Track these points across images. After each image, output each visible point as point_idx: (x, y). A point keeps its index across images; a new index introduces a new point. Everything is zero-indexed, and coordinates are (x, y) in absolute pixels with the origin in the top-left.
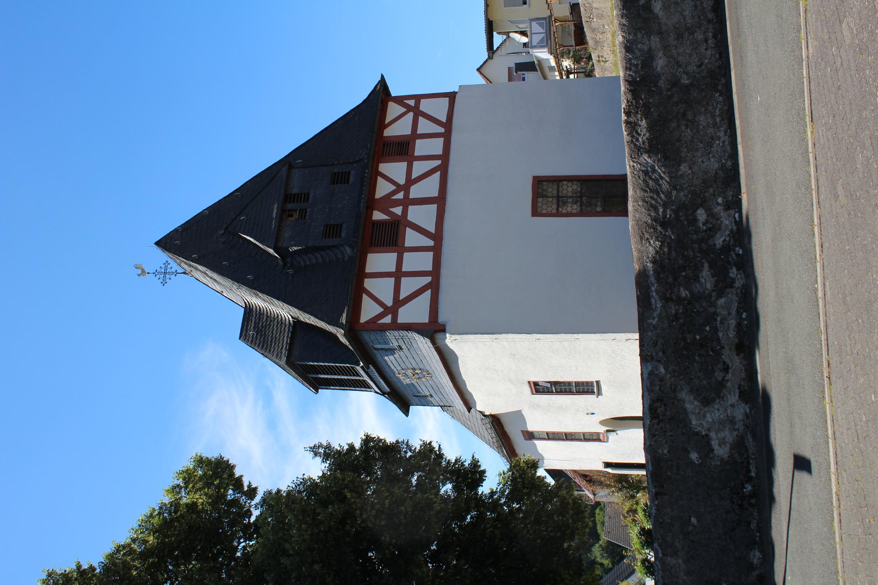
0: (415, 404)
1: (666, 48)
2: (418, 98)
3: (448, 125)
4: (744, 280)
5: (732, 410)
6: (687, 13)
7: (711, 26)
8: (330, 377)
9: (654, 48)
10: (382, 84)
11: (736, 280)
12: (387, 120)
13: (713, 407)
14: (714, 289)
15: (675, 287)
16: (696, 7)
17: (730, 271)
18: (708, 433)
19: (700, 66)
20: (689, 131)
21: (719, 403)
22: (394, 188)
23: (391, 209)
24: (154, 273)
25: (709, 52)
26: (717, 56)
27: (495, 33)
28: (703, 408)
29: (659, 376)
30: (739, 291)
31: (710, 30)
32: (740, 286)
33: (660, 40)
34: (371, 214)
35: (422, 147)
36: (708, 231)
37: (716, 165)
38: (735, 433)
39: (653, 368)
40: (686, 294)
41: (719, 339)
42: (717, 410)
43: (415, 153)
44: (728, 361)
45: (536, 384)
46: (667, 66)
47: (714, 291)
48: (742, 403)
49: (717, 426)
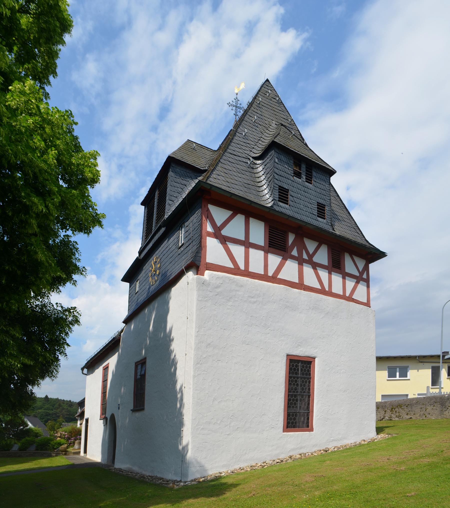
0: (129, 308)
8: (154, 221)
23: (295, 248)
24: (237, 98)
34: (293, 232)
35: (337, 279)
43: (333, 273)
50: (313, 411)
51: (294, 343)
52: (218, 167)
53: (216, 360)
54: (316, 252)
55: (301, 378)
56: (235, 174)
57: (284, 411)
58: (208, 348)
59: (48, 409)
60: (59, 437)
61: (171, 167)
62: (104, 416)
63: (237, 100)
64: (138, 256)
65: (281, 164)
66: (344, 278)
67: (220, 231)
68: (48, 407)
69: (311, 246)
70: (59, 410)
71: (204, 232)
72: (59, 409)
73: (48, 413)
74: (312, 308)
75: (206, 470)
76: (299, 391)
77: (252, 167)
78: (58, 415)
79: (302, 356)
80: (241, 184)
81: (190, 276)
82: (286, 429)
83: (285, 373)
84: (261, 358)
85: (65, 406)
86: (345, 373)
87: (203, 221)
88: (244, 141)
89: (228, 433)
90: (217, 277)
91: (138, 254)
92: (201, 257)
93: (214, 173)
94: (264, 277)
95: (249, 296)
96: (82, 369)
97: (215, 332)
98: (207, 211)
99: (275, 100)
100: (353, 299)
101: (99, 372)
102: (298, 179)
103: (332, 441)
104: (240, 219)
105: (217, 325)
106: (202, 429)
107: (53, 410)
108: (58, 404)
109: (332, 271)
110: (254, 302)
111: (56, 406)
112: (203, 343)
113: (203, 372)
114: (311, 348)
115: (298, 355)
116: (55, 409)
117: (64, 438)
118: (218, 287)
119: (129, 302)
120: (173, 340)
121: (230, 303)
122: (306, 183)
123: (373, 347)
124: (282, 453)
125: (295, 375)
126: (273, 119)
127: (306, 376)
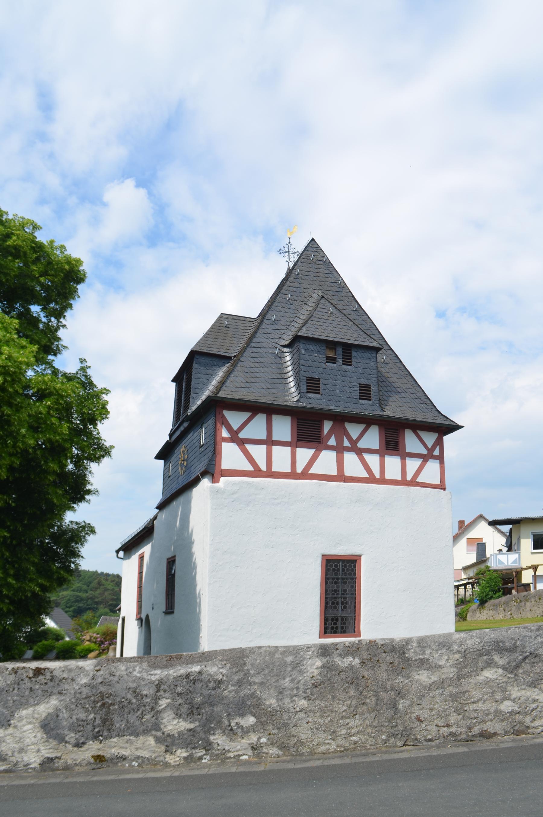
1: (441, 684)
2: (441, 458)
3: (414, 483)
4: (173, 764)
5: (35, 750)
6: (480, 704)
7: (464, 730)
9: (442, 671)
10: (453, 428)
11: (174, 756)
12: (421, 433)
13: (39, 731)
14: (166, 733)
15: (171, 694)
16: (487, 715)
17: (183, 750)
18: (12, 726)
19: (419, 719)
20: (345, 708)
21: (42, 738)
25: (435, 728)
26: (429, 737)
27: (510, 526)
28: (38, 721)
29: (78, 677)
30: (162, 758)
31: (459, 729)
32: (167, 760)
33: (451, 678)
36: (230, 728)
37: (303, 737)
38: (10, 754)
39: (87, 671)
40: (162, 705)
41: (110, 738)
42: (35, 736)
44: (86, 747)
45: (174, 561)
46: (421, 684)
47: (163, 733)
48: (40, 760)
49: (18, 735)
52: (236, 368)
53: (234, 567)
54: (363, 436)
55: (343, 579)
56: (257, 370)
57: (321, 616)
59: (80, 590)
60: (88, 641)
61: (195, 359)
62: (139, 616)
63: (289, 245)
64: (169, 439)
65: (310, 354)
66: (403, 459)
68: (79, 587)
69: (354, 430)
70: (98, 592)
71: (218, 439)
72: (98, 590)
73: (79, 596)
76: (340, 593)
77: (280, 357)
78: (96, 600)
80: (263, 380)
81: (205, 482)
83: (320, 575)
85: (109, 585)
87: (218, 428)
88: (273, 327)
91: (168, 437)
92: (215, 465)
93: (232, 375)
94: (292, 475)
96: (118, 552)
99: (321, 263)
100: (418, 482)
101: (135, 558)
102: (332, 365)
104: (261, 420)
107: (87, 592)
108: (97, 581)
109: (385, 454)
111: (94, 584)
115: (337, 554)
116: (91, 590)
117: (95, 643)
119: (163, 484)
120: (194, 542)
122: (343, 366)
123: (447, 536)
125: (335, 576)
126: (313, 287)
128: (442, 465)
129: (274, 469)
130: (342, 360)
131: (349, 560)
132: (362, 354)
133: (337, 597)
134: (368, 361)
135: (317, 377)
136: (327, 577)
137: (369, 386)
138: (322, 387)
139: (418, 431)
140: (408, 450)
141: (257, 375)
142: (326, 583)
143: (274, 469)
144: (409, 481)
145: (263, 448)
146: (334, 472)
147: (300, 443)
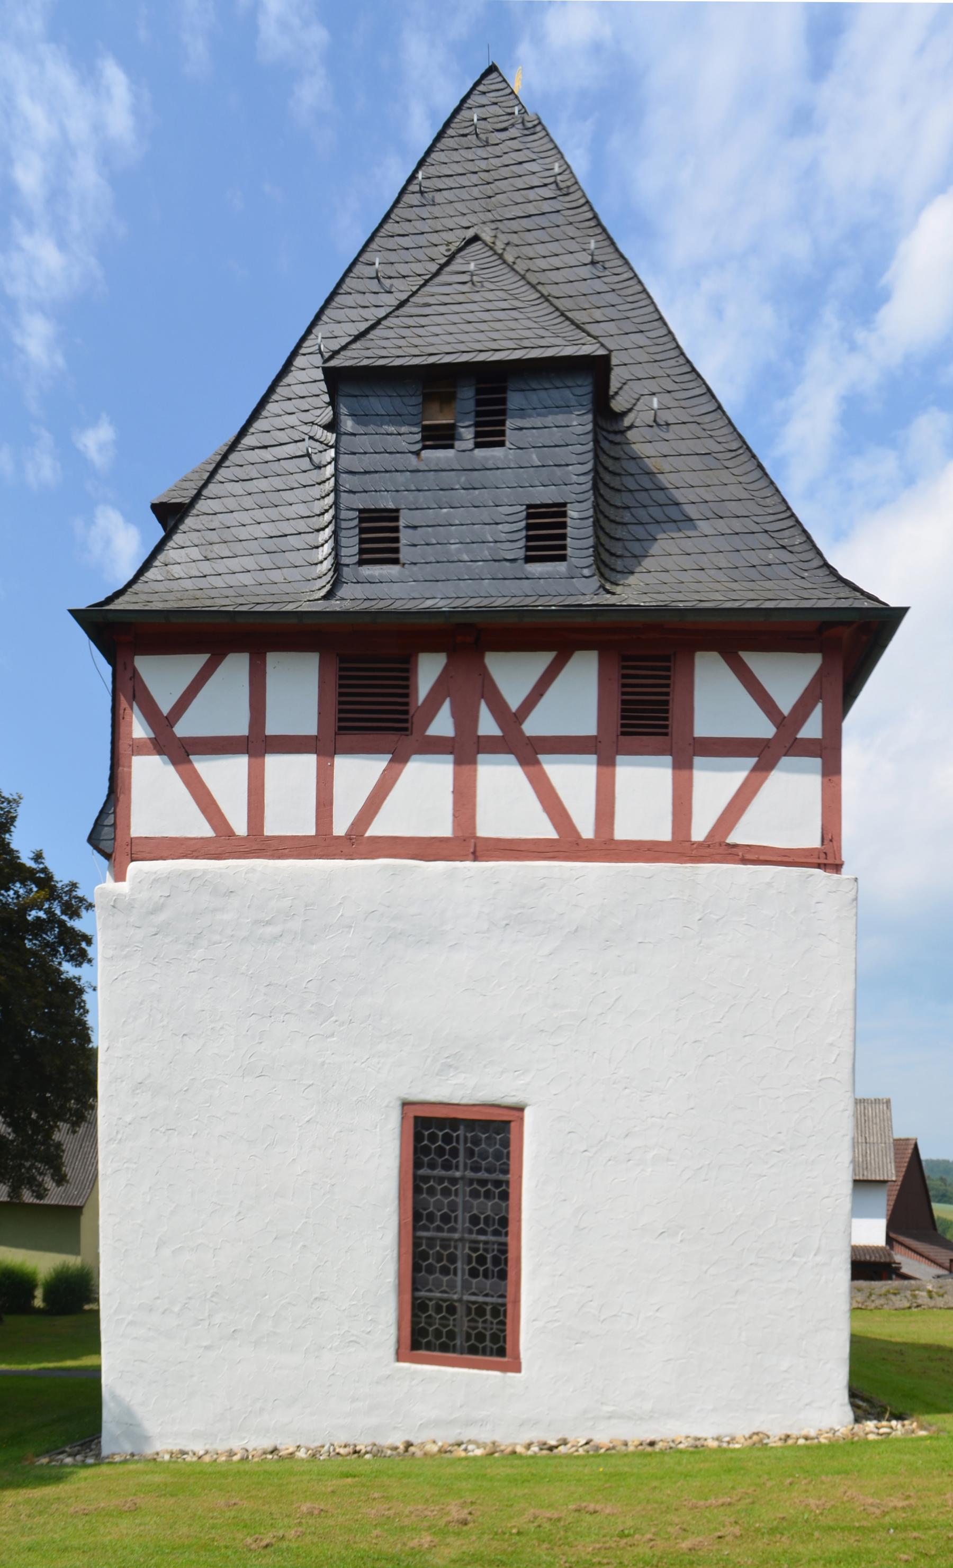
22: (165, 708)
50: (517, 1301)
51: (429, 1060)
53: (163, 1129)
54: (542, 695)
57: (400, 1293)
58: (138, 1094)
66: (683, 765)
67: (172, 727)
71: (123, 745)
74: (505, 922)
75: (146, 1439)
79: (464, 1101)
82: (408, 1351)
84: (307, 1119)
86: (668, 1160)
87: (121, 712)
89: (205, 1344)
90: (154, 880)
95: (257, 922)
97: (155, 1048)
98: (131, 679)
100: (735, 846)
103: (610, 1418)
105: (161, 1024)
106: (132, 1323)
110: (276, 938)
112: (122, 1081)
113: (126, 1165)
114: (502, 1072)
115: (446, 1100)
118: (157, 909)
121: (199, 953)
122: (477, 451)
123: (831, 1044)
124: (395, 1428)
127: (443, 1173)
128: (684, 773)
129: (270, 829)
130: (472, 430)
131: (474, 1121)
132: (543, 394)
133: (449, 1240)
134: (560, 419)
135: (391, 506)
136: (422, 1172)
137: (558, 511)
138: (405, 536)
139: (742, 654)
140: (702, 729)
141: (243, 533)
142: (417, 1190)
143: (270, 829)
144: (700, 844)
145: (239, 764)
146: (664, 834)
147: (348, 739)
